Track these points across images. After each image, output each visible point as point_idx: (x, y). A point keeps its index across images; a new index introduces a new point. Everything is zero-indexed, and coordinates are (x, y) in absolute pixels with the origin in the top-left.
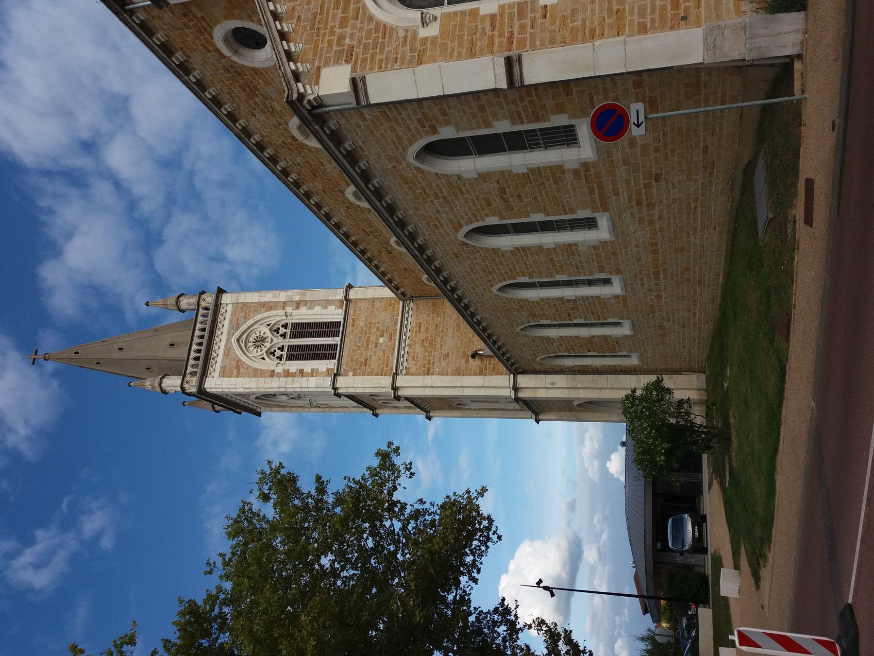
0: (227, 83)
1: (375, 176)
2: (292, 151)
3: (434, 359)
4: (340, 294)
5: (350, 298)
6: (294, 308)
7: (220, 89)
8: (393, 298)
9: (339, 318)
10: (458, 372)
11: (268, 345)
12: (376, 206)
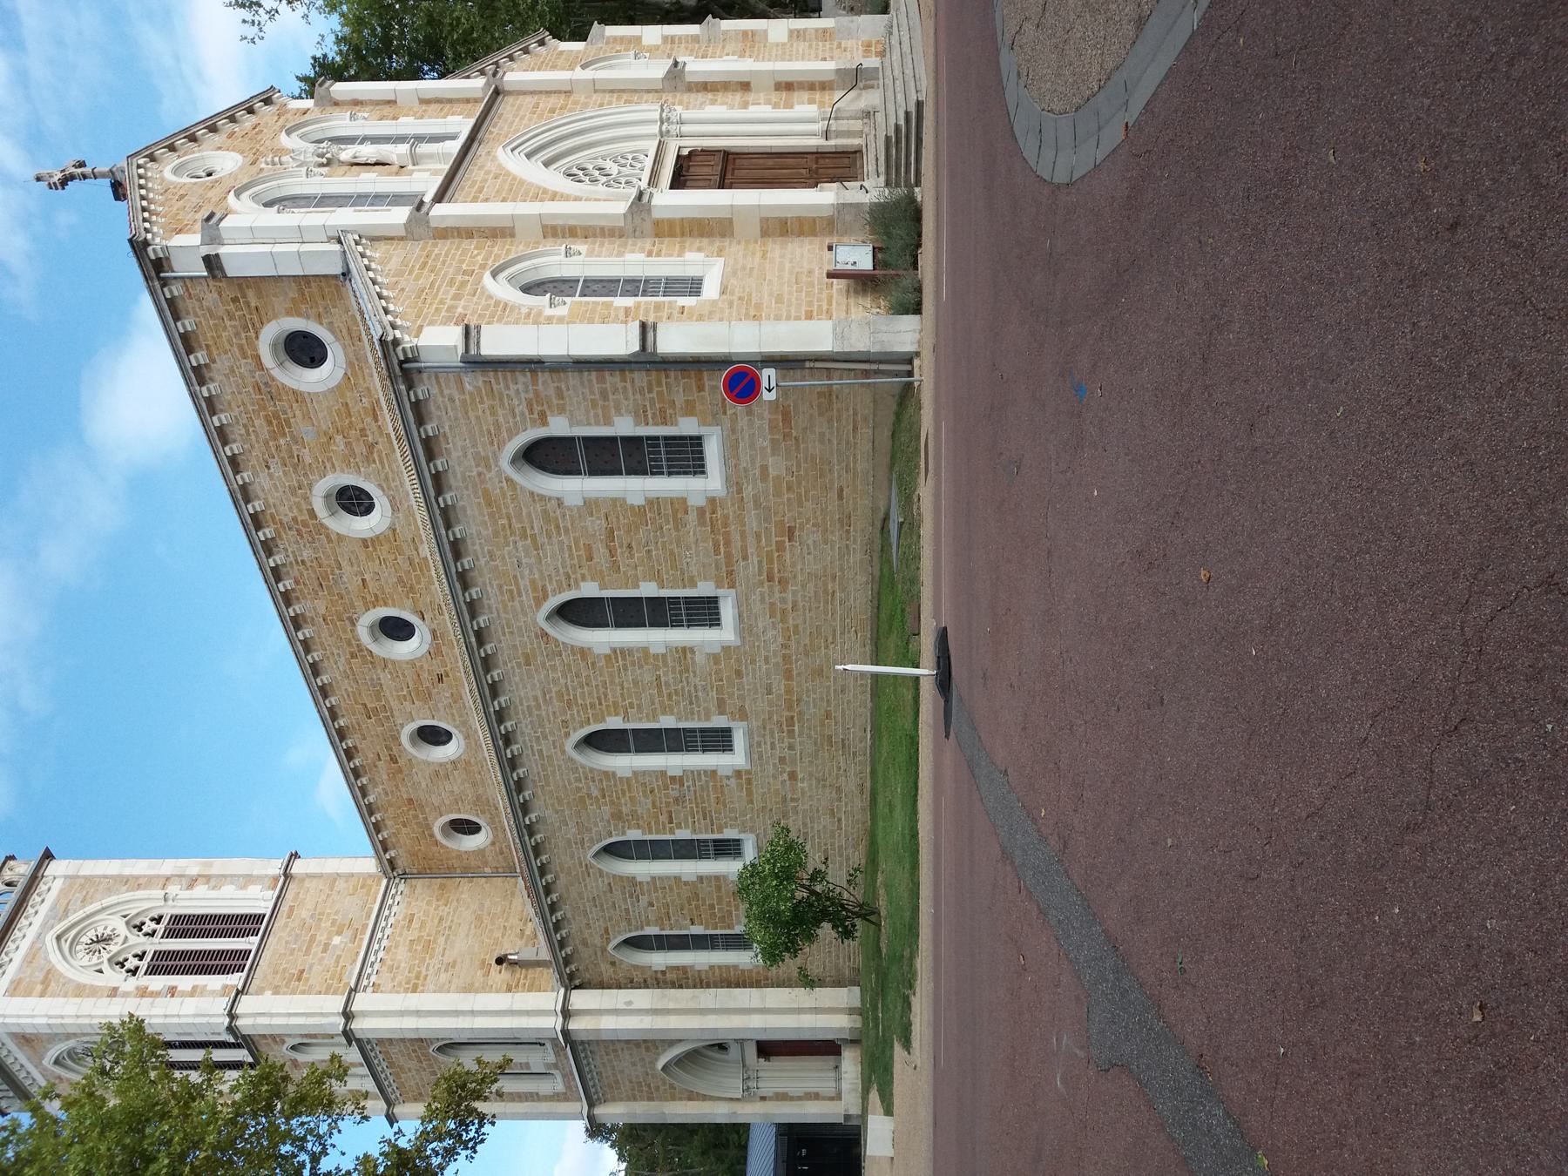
0: (250, 408)
1: (450, 488)
2: (302, 537)
3: (427, 970)
4: (275, 867)
5: (292, 871)
6: (185, 887)
7: (235, 417)
8: (370, 876)
9: (264, 908)
10: (468, 989)
11: (114, 948)
12: (440, 535)
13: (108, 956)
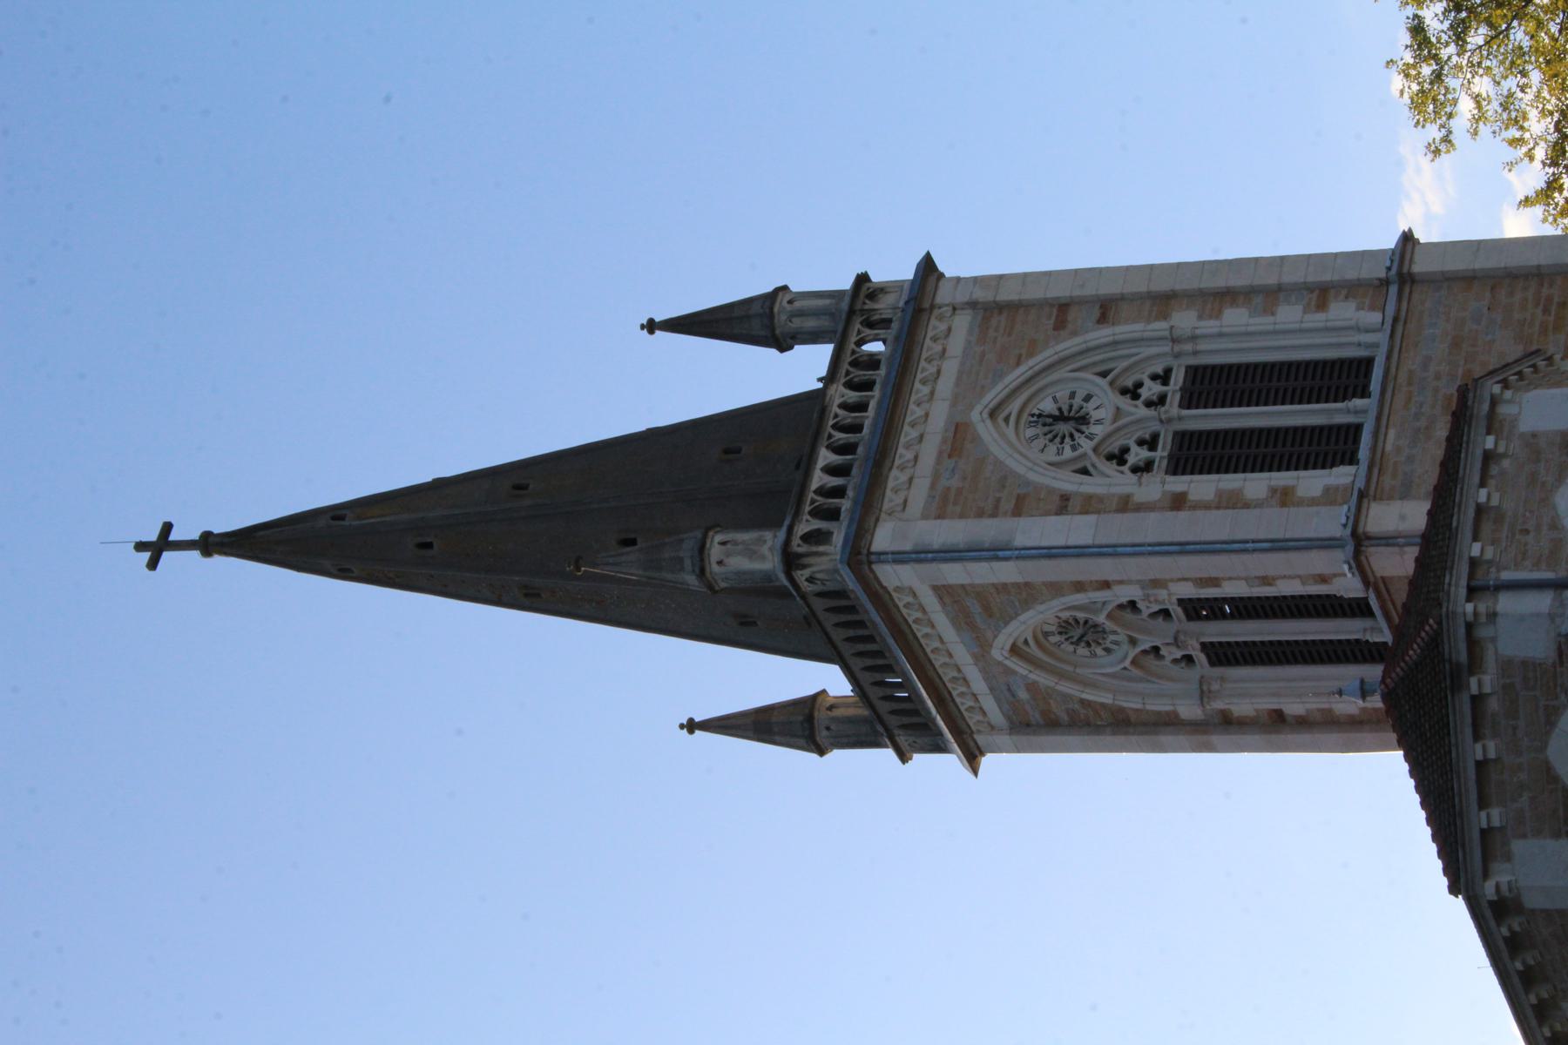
13: (1092, 444)
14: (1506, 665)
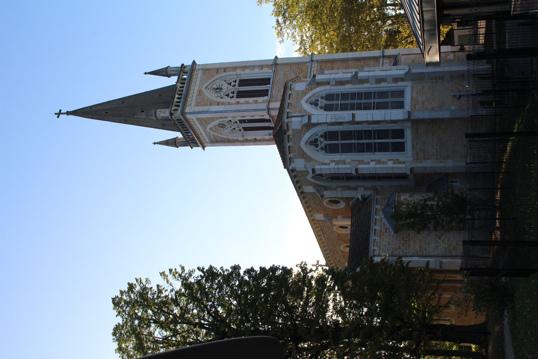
14: (293, 130)
